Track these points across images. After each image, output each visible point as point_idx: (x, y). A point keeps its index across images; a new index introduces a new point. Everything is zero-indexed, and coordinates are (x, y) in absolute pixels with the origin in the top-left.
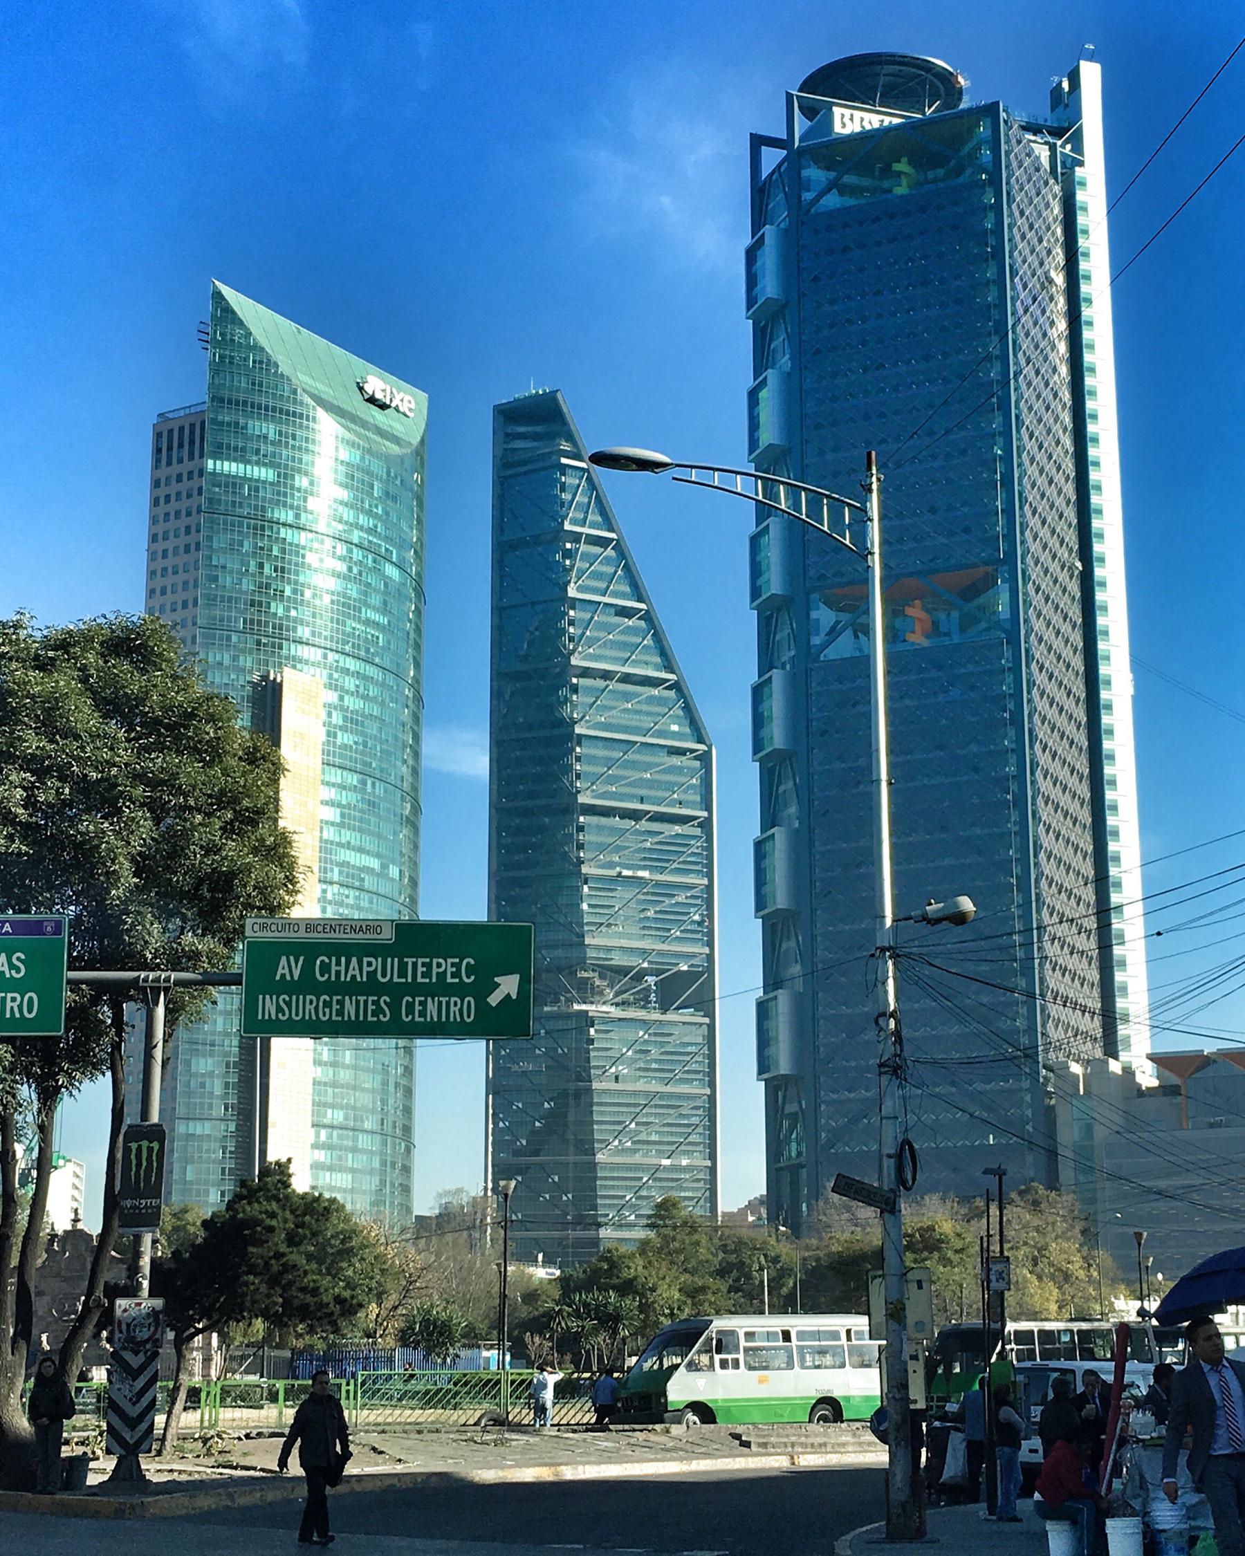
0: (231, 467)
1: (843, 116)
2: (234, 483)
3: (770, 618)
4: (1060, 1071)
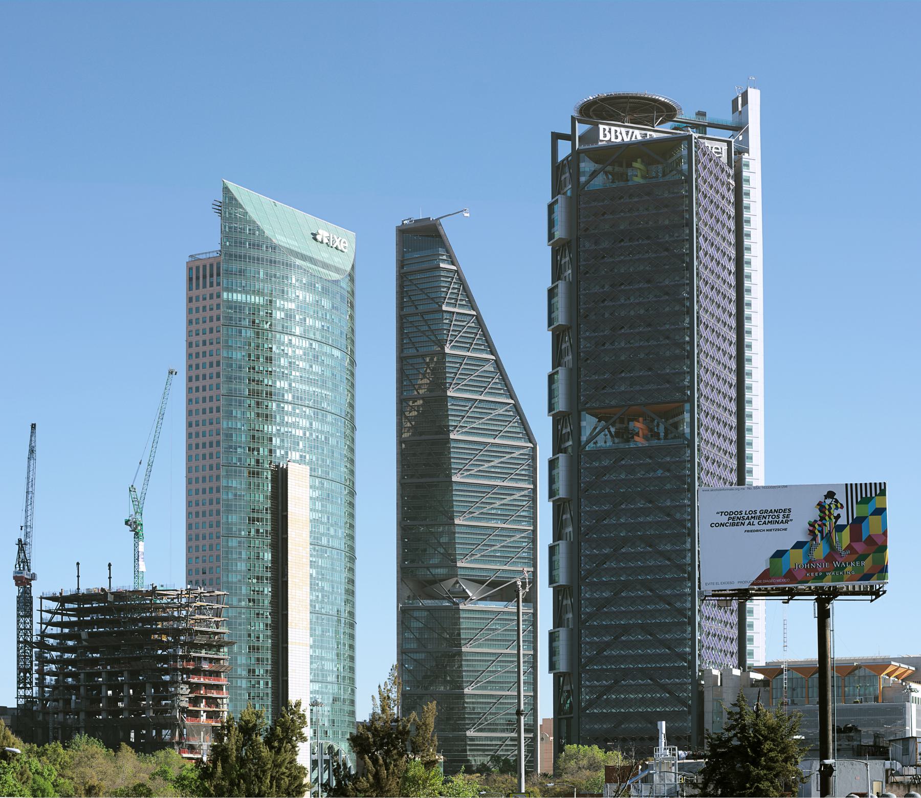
0: (238, 297)
1: (604, 130)
2: (238, 307)
3: (559, 506)
4: (706, 673)
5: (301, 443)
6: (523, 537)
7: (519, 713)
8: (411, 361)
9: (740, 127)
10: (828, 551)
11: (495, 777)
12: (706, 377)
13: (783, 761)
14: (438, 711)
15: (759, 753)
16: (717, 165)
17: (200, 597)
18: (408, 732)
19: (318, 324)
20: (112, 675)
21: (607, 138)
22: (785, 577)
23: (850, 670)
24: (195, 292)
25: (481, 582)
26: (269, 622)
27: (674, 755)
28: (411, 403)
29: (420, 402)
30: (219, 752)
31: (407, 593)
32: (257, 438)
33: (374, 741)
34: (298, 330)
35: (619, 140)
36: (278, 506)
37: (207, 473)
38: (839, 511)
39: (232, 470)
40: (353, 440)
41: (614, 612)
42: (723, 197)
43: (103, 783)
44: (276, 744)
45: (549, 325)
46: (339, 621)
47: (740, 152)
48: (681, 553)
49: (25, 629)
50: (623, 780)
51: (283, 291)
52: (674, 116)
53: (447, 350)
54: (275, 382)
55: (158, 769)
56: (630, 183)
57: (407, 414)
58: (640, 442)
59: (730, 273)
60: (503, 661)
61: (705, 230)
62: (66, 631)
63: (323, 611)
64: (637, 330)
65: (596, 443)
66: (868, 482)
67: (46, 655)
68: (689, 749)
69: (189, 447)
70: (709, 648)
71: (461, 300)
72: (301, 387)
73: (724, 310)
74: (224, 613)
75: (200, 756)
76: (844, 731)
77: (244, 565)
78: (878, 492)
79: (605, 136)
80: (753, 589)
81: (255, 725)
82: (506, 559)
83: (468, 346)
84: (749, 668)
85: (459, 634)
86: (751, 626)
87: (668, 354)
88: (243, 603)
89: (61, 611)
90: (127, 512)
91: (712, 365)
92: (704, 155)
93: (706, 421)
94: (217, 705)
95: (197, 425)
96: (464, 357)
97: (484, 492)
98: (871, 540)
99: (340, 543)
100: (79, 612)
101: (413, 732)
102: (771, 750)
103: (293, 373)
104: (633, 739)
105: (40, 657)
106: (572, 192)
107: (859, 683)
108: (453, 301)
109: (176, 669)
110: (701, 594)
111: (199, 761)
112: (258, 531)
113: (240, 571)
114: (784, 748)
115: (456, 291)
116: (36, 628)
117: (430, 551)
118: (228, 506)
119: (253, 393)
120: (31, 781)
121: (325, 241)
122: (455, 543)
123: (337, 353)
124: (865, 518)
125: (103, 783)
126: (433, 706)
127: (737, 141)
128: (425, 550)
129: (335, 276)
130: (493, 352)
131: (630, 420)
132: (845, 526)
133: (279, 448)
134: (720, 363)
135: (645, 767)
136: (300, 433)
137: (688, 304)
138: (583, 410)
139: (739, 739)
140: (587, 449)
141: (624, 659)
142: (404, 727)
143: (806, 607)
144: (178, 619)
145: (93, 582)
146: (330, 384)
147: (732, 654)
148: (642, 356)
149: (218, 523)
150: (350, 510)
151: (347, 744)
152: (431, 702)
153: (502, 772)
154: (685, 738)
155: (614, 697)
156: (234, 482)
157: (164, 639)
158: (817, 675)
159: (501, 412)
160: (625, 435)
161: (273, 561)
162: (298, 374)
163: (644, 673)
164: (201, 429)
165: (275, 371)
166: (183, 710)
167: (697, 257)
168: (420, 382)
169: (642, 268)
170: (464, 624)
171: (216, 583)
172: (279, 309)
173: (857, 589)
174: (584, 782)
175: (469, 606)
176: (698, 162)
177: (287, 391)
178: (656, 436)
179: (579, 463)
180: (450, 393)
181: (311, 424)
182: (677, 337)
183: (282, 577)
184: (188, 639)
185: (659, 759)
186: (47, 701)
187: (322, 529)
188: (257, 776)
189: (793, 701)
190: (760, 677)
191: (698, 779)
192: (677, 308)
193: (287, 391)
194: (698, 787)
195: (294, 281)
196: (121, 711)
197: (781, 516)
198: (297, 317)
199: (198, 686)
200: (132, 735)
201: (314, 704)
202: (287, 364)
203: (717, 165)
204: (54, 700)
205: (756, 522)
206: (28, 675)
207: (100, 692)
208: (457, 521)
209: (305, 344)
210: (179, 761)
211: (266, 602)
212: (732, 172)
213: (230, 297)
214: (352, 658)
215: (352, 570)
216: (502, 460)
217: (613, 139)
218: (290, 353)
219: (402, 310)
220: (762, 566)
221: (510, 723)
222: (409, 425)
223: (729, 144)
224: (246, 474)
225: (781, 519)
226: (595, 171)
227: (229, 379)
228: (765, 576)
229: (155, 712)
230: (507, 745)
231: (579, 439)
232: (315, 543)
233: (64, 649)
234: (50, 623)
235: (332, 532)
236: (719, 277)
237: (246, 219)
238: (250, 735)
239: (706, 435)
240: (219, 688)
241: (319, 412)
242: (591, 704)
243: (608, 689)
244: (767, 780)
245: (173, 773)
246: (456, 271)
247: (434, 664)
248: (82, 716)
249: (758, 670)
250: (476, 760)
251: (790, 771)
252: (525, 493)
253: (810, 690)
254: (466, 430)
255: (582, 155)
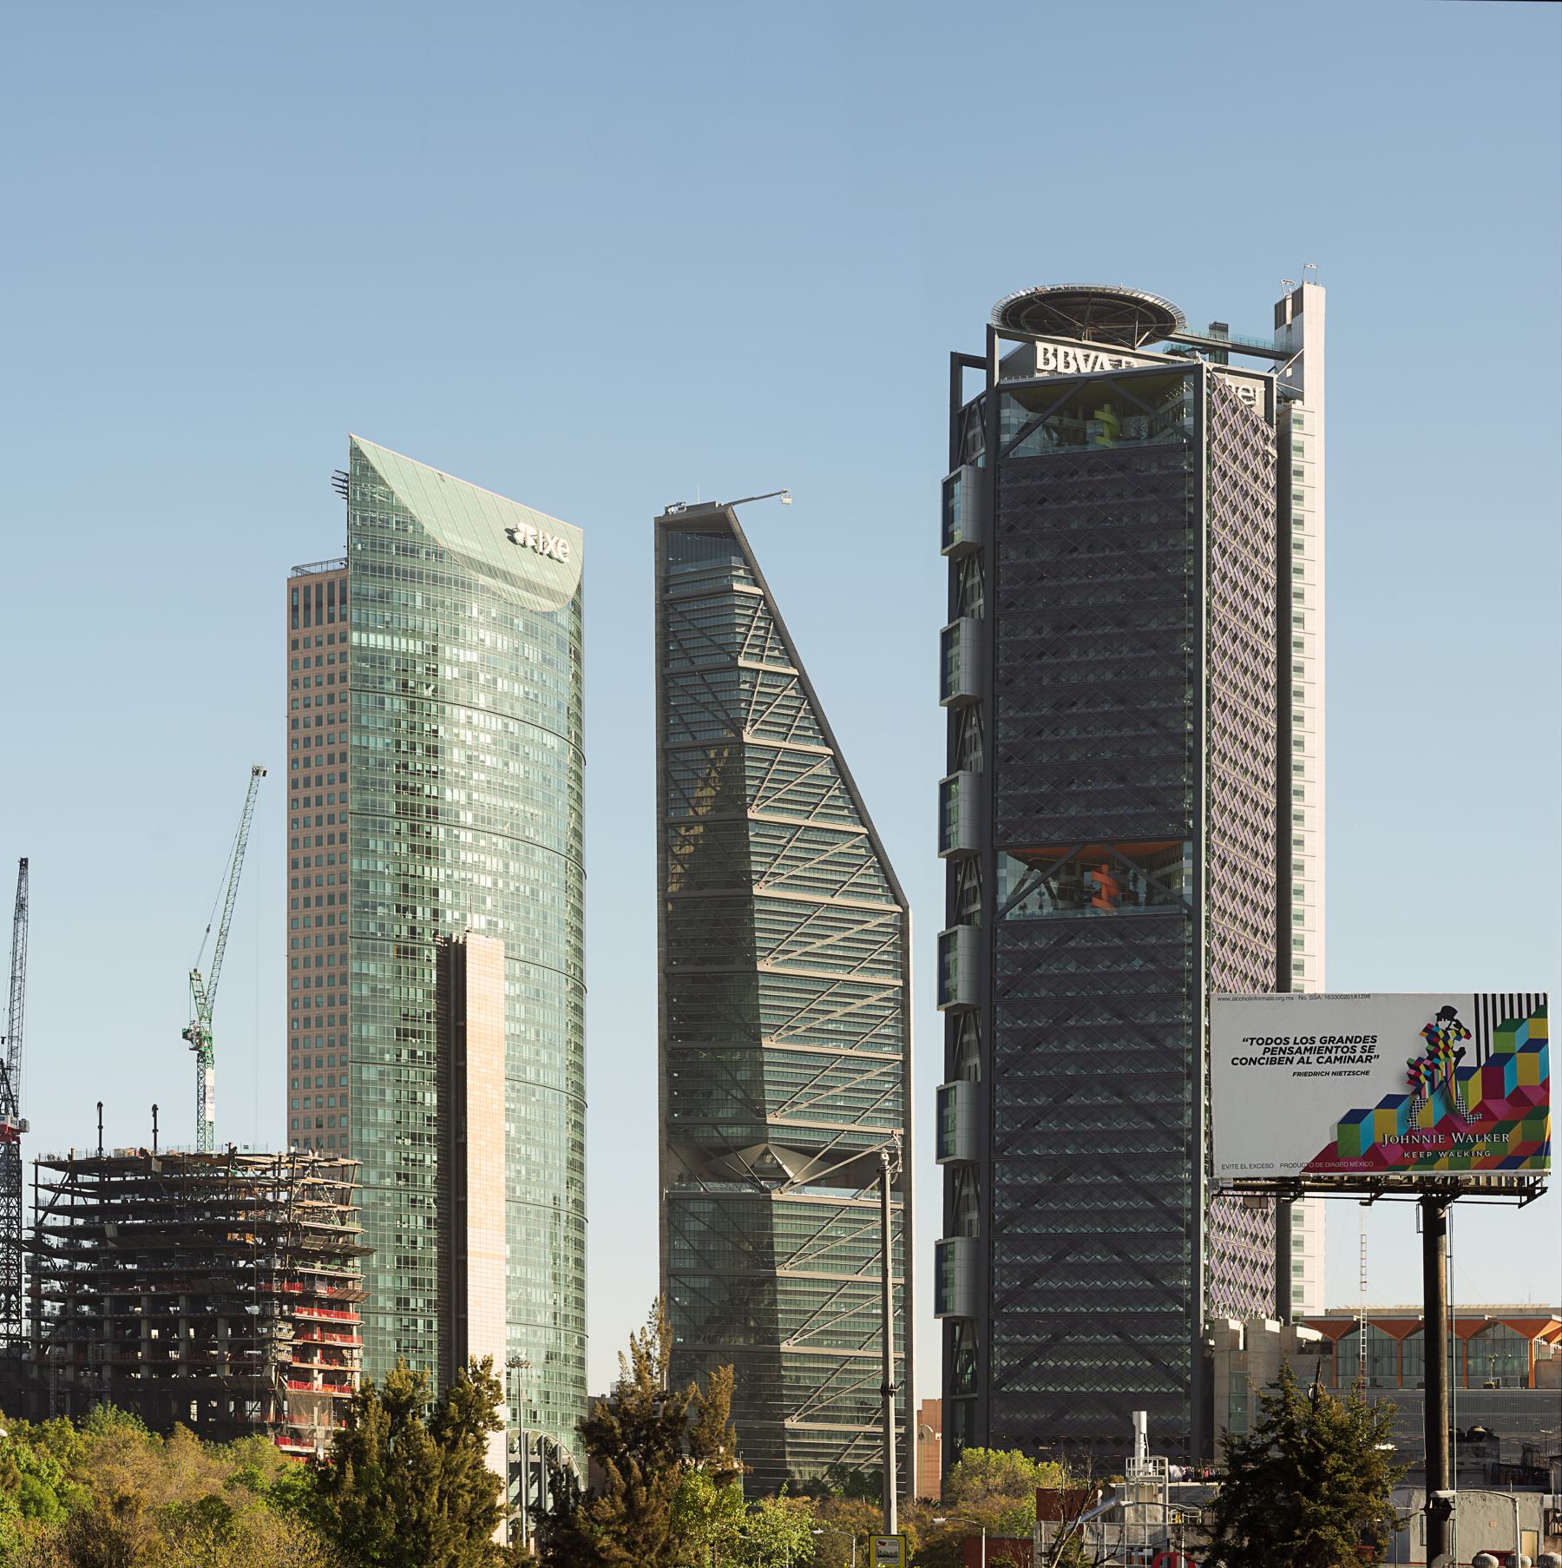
0: (378, 641)
4: (1218, 1326)
5: (489, 900)
6: (884, 1074)
7: (886, 1391)
8: (681, 756)
9: (1288, 354)
10: (1443, 1113)
11: (837, 1504)
12: (1222, 796)
13: (1361, 1490)
14: (736, 1381)
15: (1318, 1475)
16: (1246, 419)
17: (313, 1168)
18: (685, 1418)
19: (518, 690)
20: (159, 1302)
21: (1051, 367)
22: (1365, 1158)
23: (1477, 1327)
24: (302, 632)
25: (811, 1153)
26: (434, 1216)
27: (1162, 1473)
28: (682, 831)
29: (699, 830)
30: (349, 1446)
31: (678, 1169)
32: (410, 890)
33: (623, 1434)
34: (482, 700)
35: (1072, 370)
36: (448, 1011)
37: (325, 949)
38: (1464, 1043)
39: (369, 947)
40: (581, 895)
41: (1054, 1212)
42: (1256, 478)
43: (144, 1493)
44: (449, 1433)
45: (943, 696)
46: (557, 1216)
47: (1286, 398)
48: (1175, 1110)
49: (8, 1217)
50: (1071, 1515)
51: (456, 631)
52: (1172, 329)
53: (747, 738)
54: (441, 791)
55: (240, 1469)
56: (1090, 448)
57: (676, 849)
58: (1102, 908)
59: (1266, 612)
60: (850, 1296)
61: (1223, 535)
62: (80, 1222)
63: (529, 1199)
64: (1099, 710)
65: (1023, 908)
66: (1515, 993)
67: (44, 1264)
68: (1187, 1463)
69: (293, 904)
70: (1223, 1281)
71: (771, 649)
72: (488, 800)
73: (1256, 679)
74: (354, 1197)
75: (312, 1450)
76: (1466, 1438)
77: (389, 1113)
78: (1533, 1010)
79: (1047, 362)
80: (1308, 1179)
81: (412, 1398)
82: (855, 1113)
83: (784, 730)
84: (1296, 1319)
85: (771, 1245)
86: (1300, 1243)
87: (1154, 753)
88: (388, 1182)
89: (71, 1188)
90: (187, 1015)
91: (1233, 776)
92: (1223, 401)
93: (1221, 874)
94: (342, 1361)
95: (307, 865)
96: (777, 750)
97: (815, 992)
98: (1519, 1096)
99: (558, 1078)
100: (101, 1190)
101: (694, 1418)
102: (1338, 1470)
103: (475, 775)
104: (1086, 1442)
105: (33, 1267)
106: (986, 461)
107: (1493, 1351)
108: (756, 651)
109: (271, 1295)
110: (1213, 1183)
111: (311, 1458)
112: (413, 1054)
113: (383, 1125)
114: (1363, 1467)
115: (761, 633)
116: (28, 1217)
117: (718, 1094)
118: (361, 1008)
119: (405, 810)
120: (19, 1486)
121: (530, 543)
122: (763, 1082)
123: (551, 741)
124: (1509, 1056)
125: (144, 1493)
126: (728, 1372)
127: (1282, 378)
128: (710, 1093)
129: (547, 605)
130: (829, 741)
131: (1085, 869)
132: (1472, 1071)
133: (451, 907)
134: (1246, 771)
135: (1110, 1493)
136: (486, 881)
137: (1191, 665)
138: (1003, 848)
139: (1282, 1448)
140: (1008, 917)
141: (1069, 1296)
142: (678, 1409)
143: (1400, 1216)
144: (275, 1206)
145: (126, 1138)
146: (539, 796)
147: (1265, 1293)
148: (1107, 755)
149: (344, 1037)
150: (576, 1019)
151: (572, 1437)
152: (725, 1366)
153: (850, 1494)
154: (1180, 1442)
155: (1067, 1363)
156: (372, 966)
157: (250, 1241)
158: (1422, 1333)
159: (844, 849)
160: (1075, 895)
161: (439, 1108)
162: (482, 777)
163: (1107, 1323)
164: (313, 871)
165: (443, 772)
166: (283, 1368)
167: (1208, 583)
168: (699, 794)
169: (1109, 598)
170: (780, 1227)
171: (340, 1144)
172: (450, 662)
173: (1494, 1183)
174: (997, 1516)
175: (788, 1195)
176: (1212, 413)
177: (463, 807)
178: (1132, 898)
179: (993, 942)
180: (750, 815)
181: (506, 866)
182: (1171, 724)
183: (457, 1136)
184: (292, 1242)
185: (1134, 1480)
186: (47, 1343)
187: (527, 1052)
188: (414, 1488)
189: (1374, 1381)
190: (1315, 1335)
191: (1210, 1518)
192: (1171, 672)
193: (463, 807)
194: (1207, 1532)
195: (475, 614)
196: (174, 1366)
197: (1359, 1049)
198: (482, 676)
199: (309, 1324)
200: (194, 1408)
201: (514, 1363)
202: (463, 760)
203: (1246, 419)
204: (58, 1344)
205: (1313, 1058)
206: (13, 1298)
207: (137, 1332)
208: (766, 1043)
209: (496, 723)
210: (274, 1459)
211: (428, 1180)
212: (1272, 433)
213: (364, 641)
214: (580, 1284)
215: (579, 1126)
216: (847, 934)
217: (1061, 369)
218: (469, 741)
219: (667, 666)
220: (1324, 1138)
221: (863, 1407)
222: (679, 869)
223: (1268, 382)
224: (392, 954)
225: (1358, 1055)
226: (1027, 424)
227: (363, 785)
228: (1328, 1156)
229: (234, 1369)
230: (857, 1447)
231: (995, 899)
232: (514, 1079)
233: (74, 1254)
234: (52, 1209)
235: (544, 1058)
236: (1246, 619)
237: (390, 503)
238: (404, 1417)
239: (1221, 900)
240: (345, 1329)
241: (522, 843)
242: (1009, 1375)
243: (1041, 1351)
244: (1332, 1523)
245: (266, 1479)
246: (763, 598)
247: (727, 1297)
248: (107, 1373)
249: (1312, 1323)
250: (803, 1472)
251: (1373, 1509)
252: (889, 993)
253: (1406, 1361)
254: (781, 879)
255: (1005, 395)
